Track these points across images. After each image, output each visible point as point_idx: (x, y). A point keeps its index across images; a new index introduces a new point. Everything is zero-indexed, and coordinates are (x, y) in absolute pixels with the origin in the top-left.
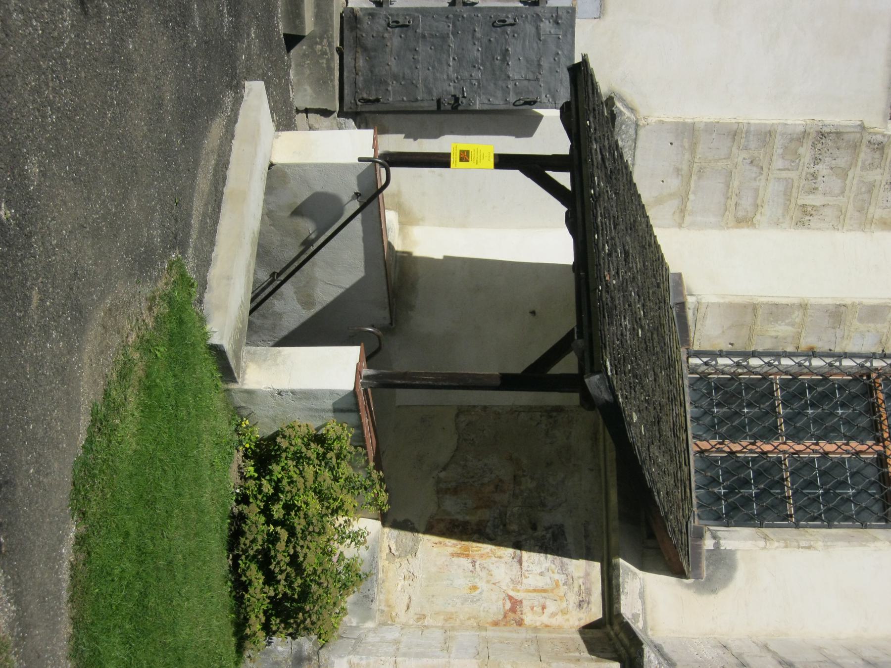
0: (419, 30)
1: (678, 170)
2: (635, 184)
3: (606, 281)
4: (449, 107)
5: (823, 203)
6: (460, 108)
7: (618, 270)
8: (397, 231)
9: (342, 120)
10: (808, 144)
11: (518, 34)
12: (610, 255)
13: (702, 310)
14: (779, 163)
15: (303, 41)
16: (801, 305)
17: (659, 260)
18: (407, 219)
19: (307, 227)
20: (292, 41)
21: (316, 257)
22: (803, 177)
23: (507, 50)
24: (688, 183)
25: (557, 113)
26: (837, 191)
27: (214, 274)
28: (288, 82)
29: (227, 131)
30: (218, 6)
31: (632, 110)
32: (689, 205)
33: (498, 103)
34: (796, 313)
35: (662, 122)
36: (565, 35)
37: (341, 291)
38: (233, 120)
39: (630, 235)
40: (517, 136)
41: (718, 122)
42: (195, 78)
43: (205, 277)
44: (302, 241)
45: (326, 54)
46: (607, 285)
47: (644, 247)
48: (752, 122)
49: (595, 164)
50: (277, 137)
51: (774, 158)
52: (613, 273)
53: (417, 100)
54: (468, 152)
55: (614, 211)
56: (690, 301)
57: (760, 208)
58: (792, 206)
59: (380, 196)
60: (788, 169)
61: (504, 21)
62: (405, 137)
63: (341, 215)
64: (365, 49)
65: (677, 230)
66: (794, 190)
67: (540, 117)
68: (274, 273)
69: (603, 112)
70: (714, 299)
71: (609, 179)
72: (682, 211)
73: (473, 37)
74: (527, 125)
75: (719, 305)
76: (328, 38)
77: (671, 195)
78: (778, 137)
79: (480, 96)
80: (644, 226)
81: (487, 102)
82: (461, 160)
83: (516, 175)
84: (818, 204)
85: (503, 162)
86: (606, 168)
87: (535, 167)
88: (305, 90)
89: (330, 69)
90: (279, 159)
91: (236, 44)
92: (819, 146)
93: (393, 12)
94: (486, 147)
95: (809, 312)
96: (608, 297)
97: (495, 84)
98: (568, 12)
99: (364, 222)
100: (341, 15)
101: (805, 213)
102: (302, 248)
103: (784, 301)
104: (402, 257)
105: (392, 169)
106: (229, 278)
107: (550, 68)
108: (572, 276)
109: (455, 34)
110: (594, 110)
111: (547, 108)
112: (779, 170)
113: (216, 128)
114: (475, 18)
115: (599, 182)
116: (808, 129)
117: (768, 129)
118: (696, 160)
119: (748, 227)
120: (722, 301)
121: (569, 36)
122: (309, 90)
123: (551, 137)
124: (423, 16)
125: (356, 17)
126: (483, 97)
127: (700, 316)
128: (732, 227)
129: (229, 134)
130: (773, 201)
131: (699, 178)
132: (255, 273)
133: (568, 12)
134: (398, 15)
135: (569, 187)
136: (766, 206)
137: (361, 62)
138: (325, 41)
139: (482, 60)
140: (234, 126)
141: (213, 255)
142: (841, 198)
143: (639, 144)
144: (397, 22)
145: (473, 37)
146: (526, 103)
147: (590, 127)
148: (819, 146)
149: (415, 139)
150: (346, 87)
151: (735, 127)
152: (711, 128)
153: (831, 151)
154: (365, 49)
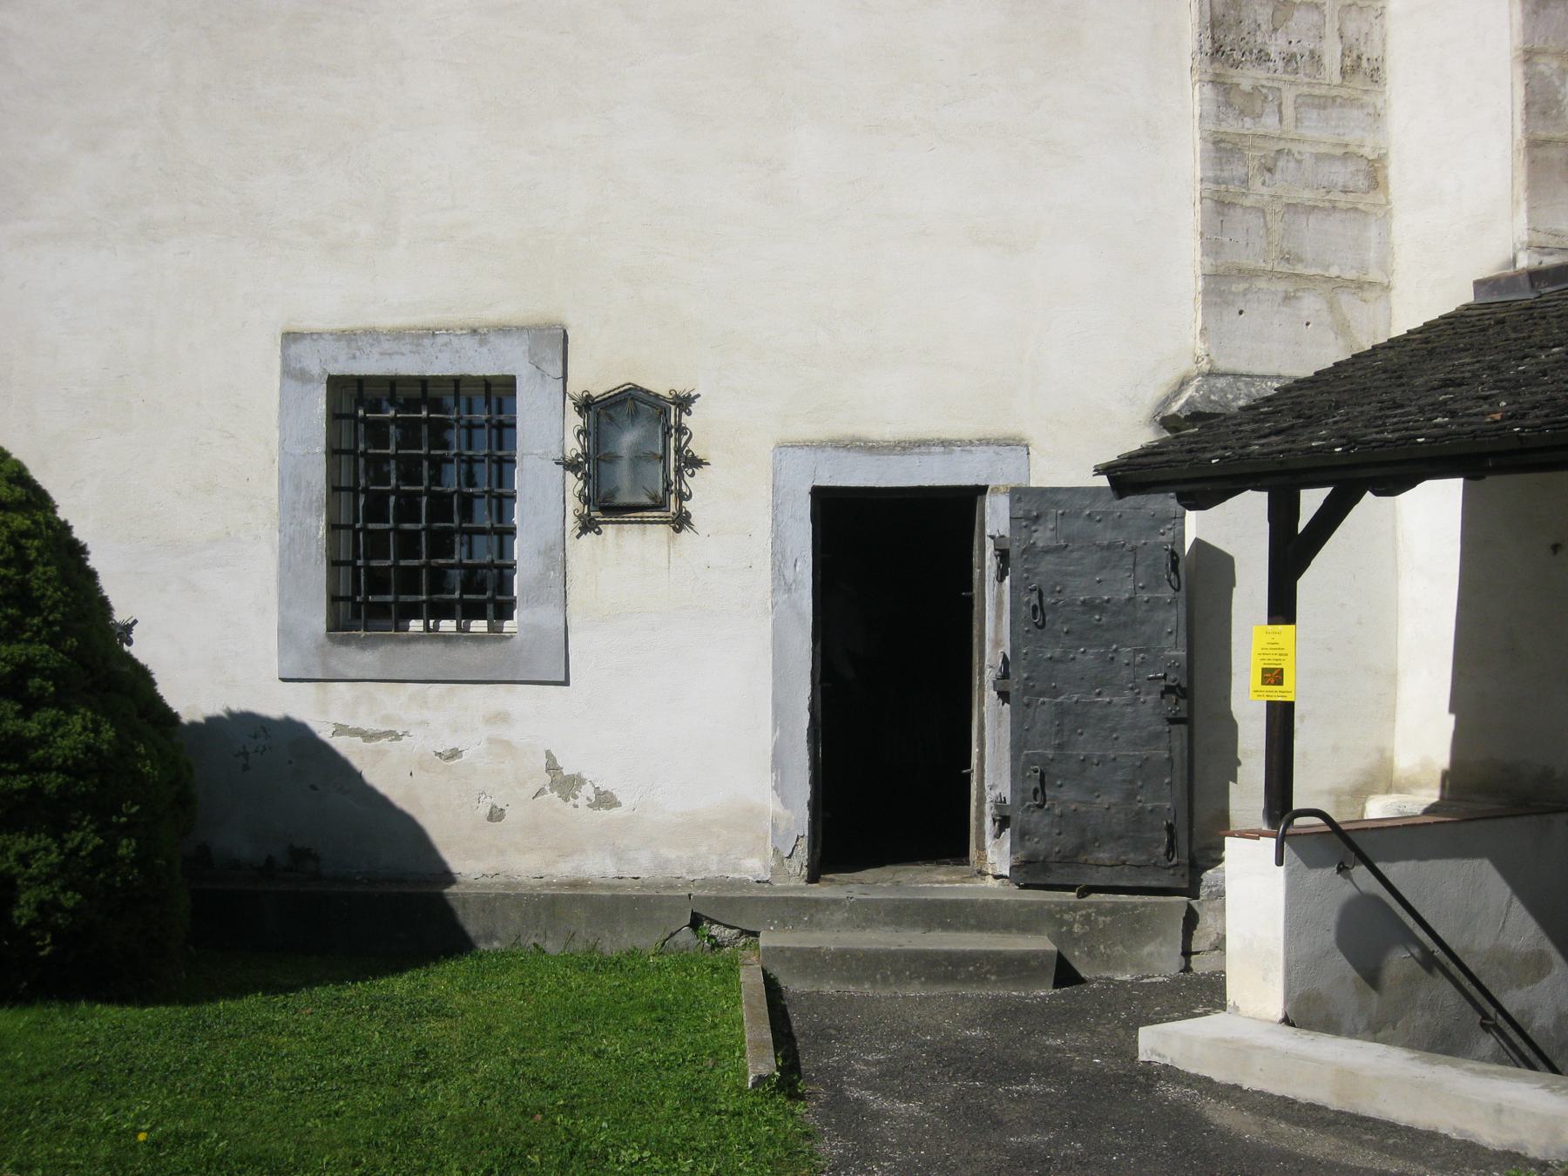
0: (1050, 753)
1: (1287, 298)
2: (1317, 373)
3: (1503, 419)
4: (1183, 703)
5: (1337, 39)
6: (1184, 684)
7: (1479, 398)
8: (1403, 797)
9: (1203, 892)
10: (1235, 76)
11: (1057, 584)
12: (1453, 414)
13: (1542, 239)
14: (1270, 122)
15: (1066, 954)
16: (1526, 61)
17: (1451, 322)
18: (1381, 779)
19: (1400, 961)
20: (1065, 975)
21: (1453, 947)
22: (1292, 78)
23: (1084, 602)
24: (1309, 278)
25: (1191, 517)
26: (1315, 17)
27: (1490, 1136)
28: (1135, 984)
29: (1227, 1098)
30: (1012, 1100)
31: (1183, 384)
32: (1351, 274)
33: (1174, 618)
34: (1542, 68)
35: (1204, 331)
36: (1057, 504)
37: (1517, 903)
38: (1206, 1085)
39: (1412, 377)
40: (1233, 584)
41: (1202, 234)
42: (1135, 1149)
43: (1496, 1154)
44: (1424, 972)
45: (1089, 915)
46: (1510, 418)
47: (1431, 352)
48: (1199, 175)
49: (1287, 446)
50: (1236, 1008)
51: (1261, 131)
52: (1486, 407)
53: (1170, 759)
54: (1264, 671)
55: (1371, 409)
56: (1524, 262)
57: (1350, 149)
58: (1344, 92)
59: (1344, 827)
60: (1280, 105)
61: (1035, 608)
62: (1235, 781)
63: (1377, 900)
64: (1082, 848)
65: (1393, 293)
66: (1317, 92)
67: (1198, 543)
68: (1482, 1025)
69: (1193, 435)
70: (1522, 219)
71: (1311, 421)
72: (1360, 286)
73: (1060, 661)
74: (1214, 567)
75: (1531, 209)
76: (1061, 912)
77: (1332, 307)
78: (1224, 127)
79: (1163, 650)
80: (1391, 353)
81: (1173, 637)
82: (1279, 682)
83: (1307, 586)
84: (1339, 48)
85: (1282, 608)
86: (1292, 426)
87: (1292, 553)
88: (1151, 954)
89: (1115, 910)
90: (1275, 1007)
91: (1075, 1073)
92: (1237, 55)
93: (1019, 798)
94: (1253, 639)
95: (1538, 44)
96: (1533, 413)
97: (1142, 623)
98: (1019, 500)
99: (1393, 859)
100: (1022, 887)
101: (1355, 68)
102: (1438, 972)
103: (1520, 92)
104: (1452, 788)
105: (1296, 806)
106: (1499, 1110)
107: (1114, 528)
108: (1491, 482)
109: (1056, 693)
110: (1190, 451)
111: (1182, 533)
112: (1281, 121)
113: (1224, 1116)
114: (1029, 657)
115: (1319, 439)
116: (1207, 78)
117: (1210, 146)
118: (1269, 268)
119: (1385, 167)
120: (1524, 206)
121: (1060, 497)
122: (1147, 950)
123: (1238, 526)
124: (1025, 747)
125: (1026, 863)
126: (1165, 644)
127: (1553, 243)
128: (1386, 196)
129: (1232, 1093)
130: (1337, 126)
131: (1300, 260)
132: (1481, 1059)
133: (1019, 500)
134: (1024, 791)
135: (1327, 491)
136: (1347, 139)
137: (1104, 856)
138: (1066, 917)
139: (1101, 646)
140: (1218, 1084)
141: (1454, 1136)
142: (1327, 9)
143: (1242, 368)
144: (1036, 791)
145: (1060, 661)
146: (1175, 568)
147: (1222, 458)
148: (1237, 55)
149: (1239, 763)
150: (1146, 883)
151: (1208, 203)
152: (1212, 244)
153: (1244, 34)
154: (1082, 848)
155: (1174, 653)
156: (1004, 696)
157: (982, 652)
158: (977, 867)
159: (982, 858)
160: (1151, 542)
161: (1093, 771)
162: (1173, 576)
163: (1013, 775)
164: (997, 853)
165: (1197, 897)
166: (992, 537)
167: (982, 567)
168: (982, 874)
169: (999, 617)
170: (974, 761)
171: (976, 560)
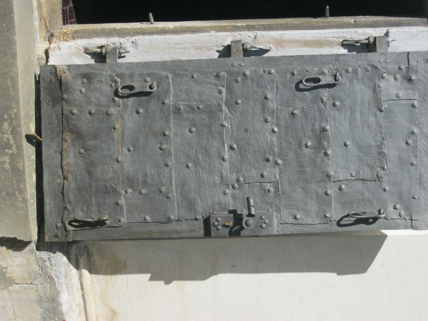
0: (170, 101)
6: (243, 233)
9: (44, 255)
11: (342, 102)
23: (324, 130)
33: (311, 220)
45: (10, 148)
53: (169, 221)
62: (151, 279)
64: (78, 136)
73: (264, 107)
79: (278, 210)
81: (291, 220)
89: (18, 173)
93: (124, 71)
97: (305, 189)
109: (232, 104)
114: (266, 76)
124: (176, 75)
134: (131, 76)
137: (71, 159)
139: (281, 148)
144: (131, 88)
145: (264, 107)
154: (78, 136)
155: (275, 221)
156: (226, 52)
157: (270, 28)
158: (56, 32)
159: (66, 37)
160: (386, 196)
161: (154, 145)
162: (353, 219)
163: (146, 65)
164: (70, 50)
165: (38, 248)
166: (387, 34)
167: (356, 25)
168: (51, 37)
169: (307, 43)
170: (161, 25)
171: (361, 19)
